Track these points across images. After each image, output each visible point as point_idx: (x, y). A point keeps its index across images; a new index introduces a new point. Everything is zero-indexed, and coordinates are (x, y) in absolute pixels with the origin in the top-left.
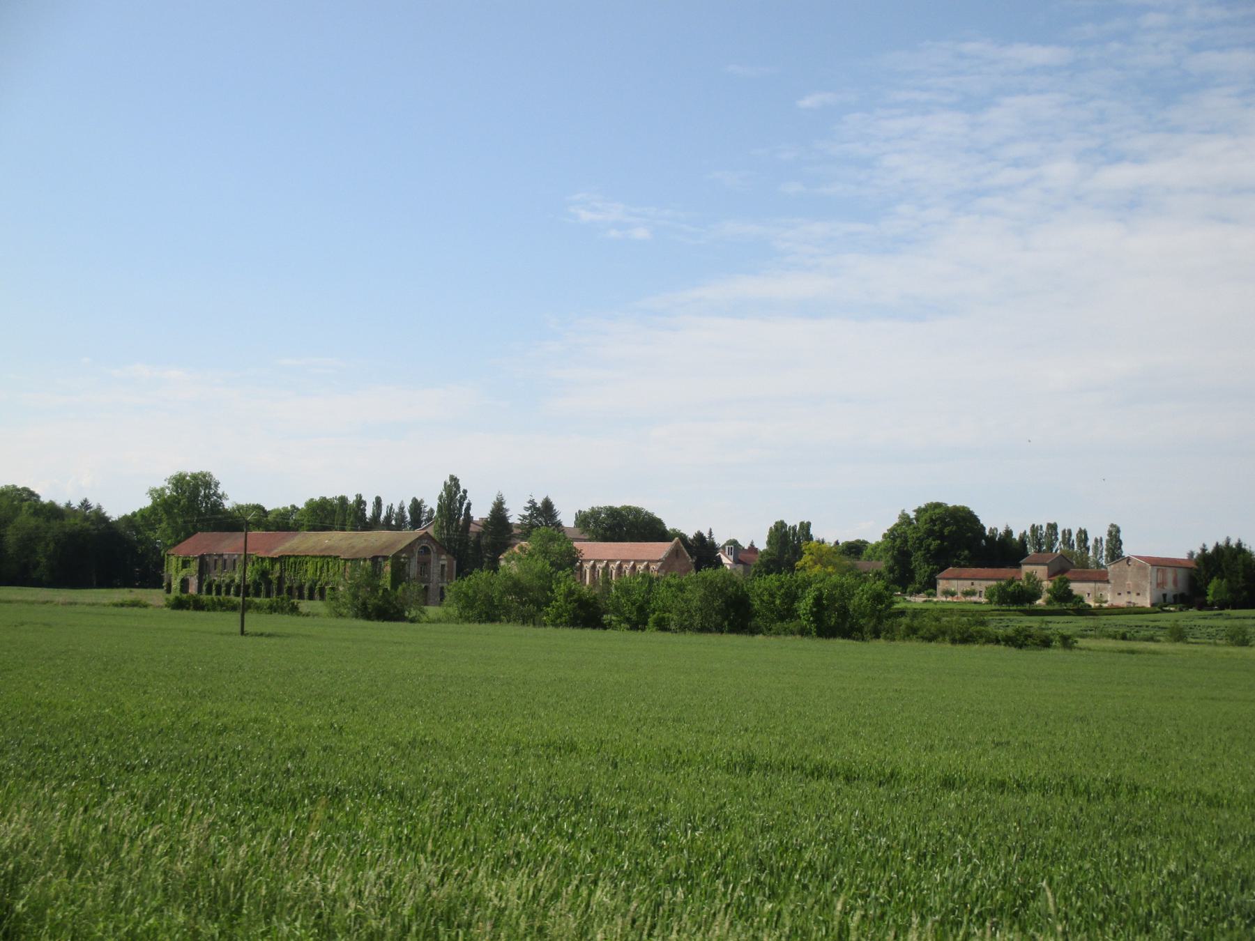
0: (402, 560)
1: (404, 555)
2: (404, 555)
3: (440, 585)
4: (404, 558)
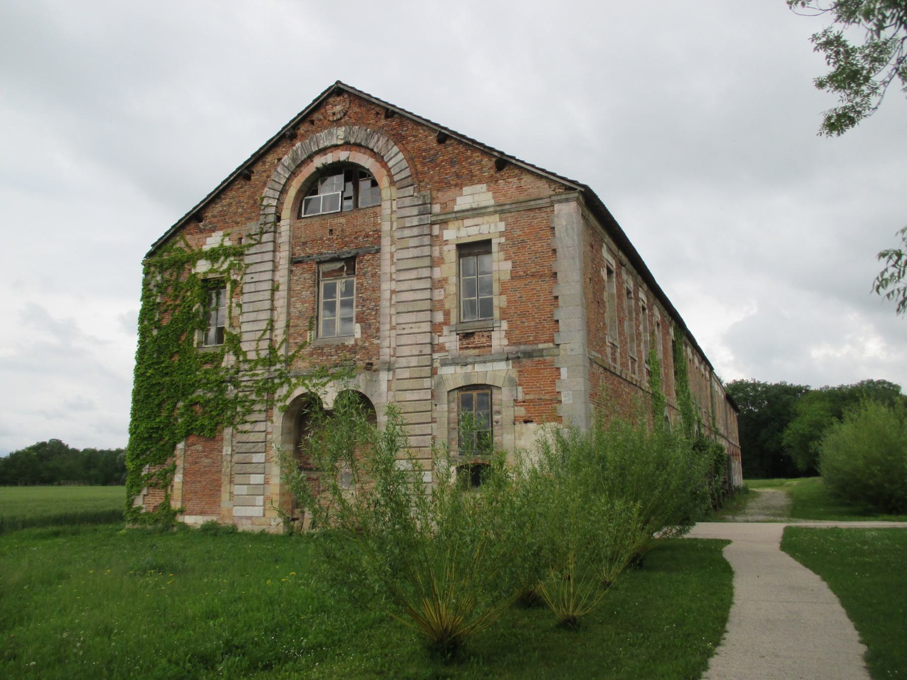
0: (202, 267)
1: (213, 241)
2: (213, 241)
3: (454, 376)
4: (213, 256)
